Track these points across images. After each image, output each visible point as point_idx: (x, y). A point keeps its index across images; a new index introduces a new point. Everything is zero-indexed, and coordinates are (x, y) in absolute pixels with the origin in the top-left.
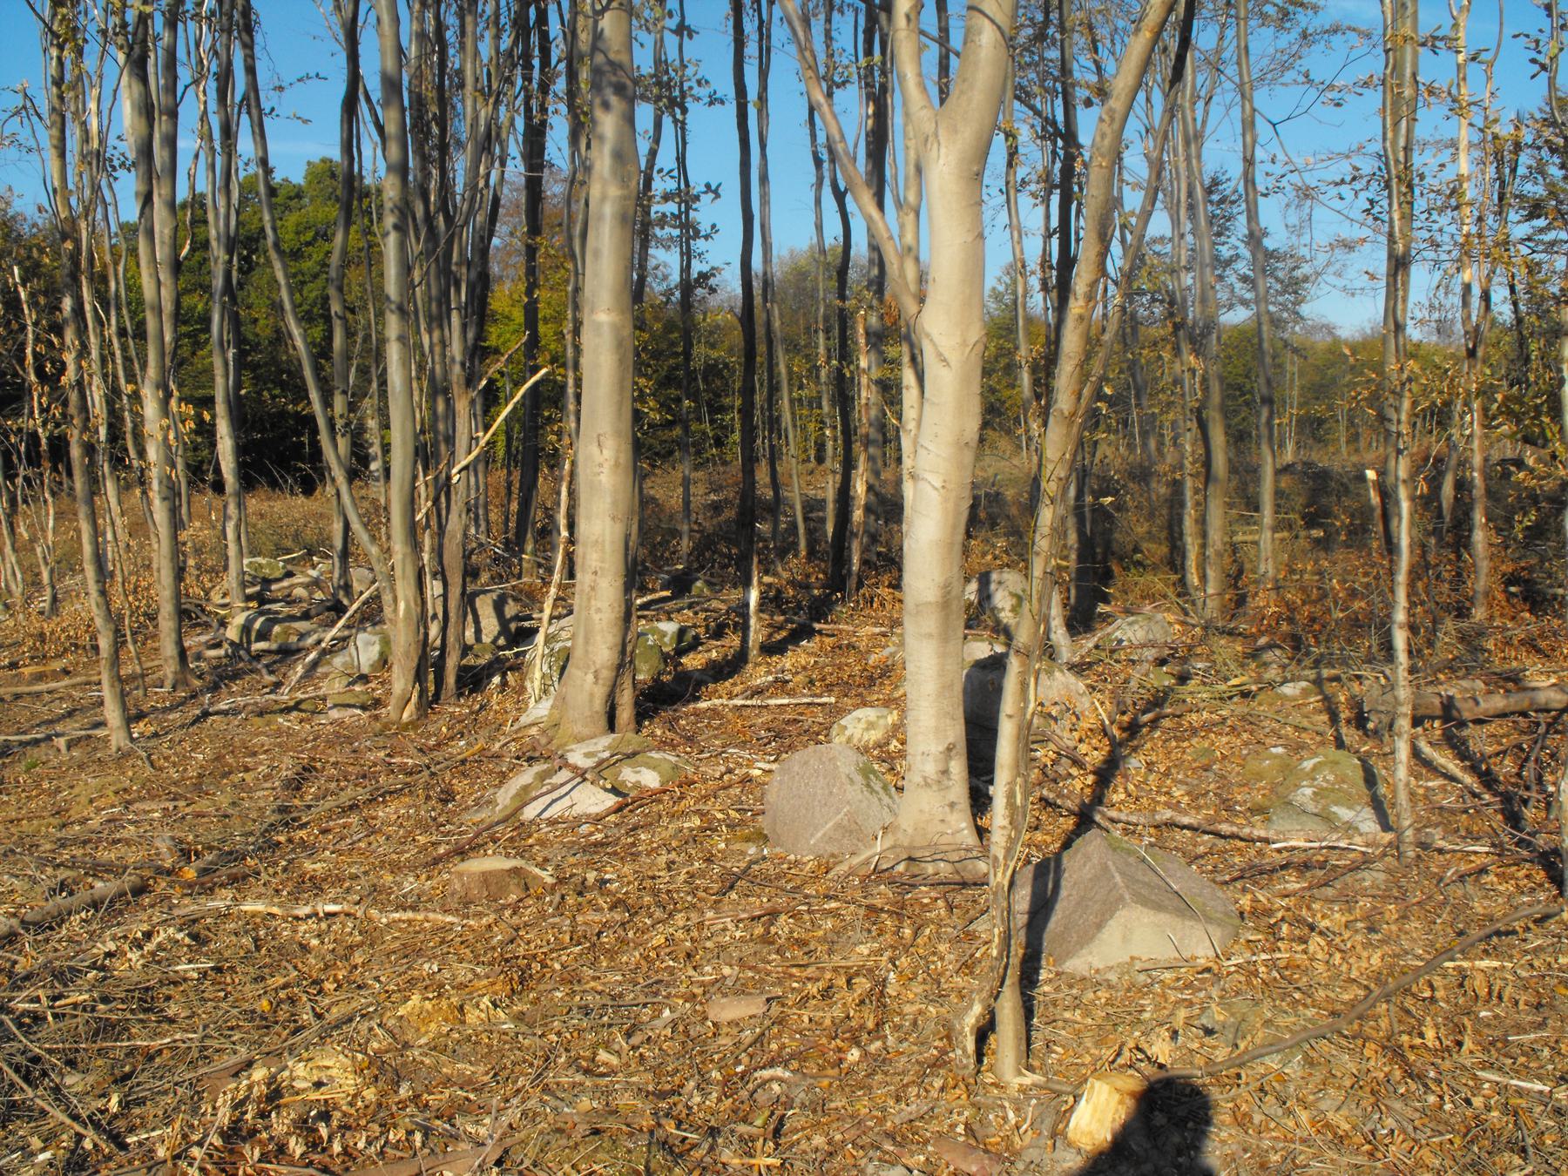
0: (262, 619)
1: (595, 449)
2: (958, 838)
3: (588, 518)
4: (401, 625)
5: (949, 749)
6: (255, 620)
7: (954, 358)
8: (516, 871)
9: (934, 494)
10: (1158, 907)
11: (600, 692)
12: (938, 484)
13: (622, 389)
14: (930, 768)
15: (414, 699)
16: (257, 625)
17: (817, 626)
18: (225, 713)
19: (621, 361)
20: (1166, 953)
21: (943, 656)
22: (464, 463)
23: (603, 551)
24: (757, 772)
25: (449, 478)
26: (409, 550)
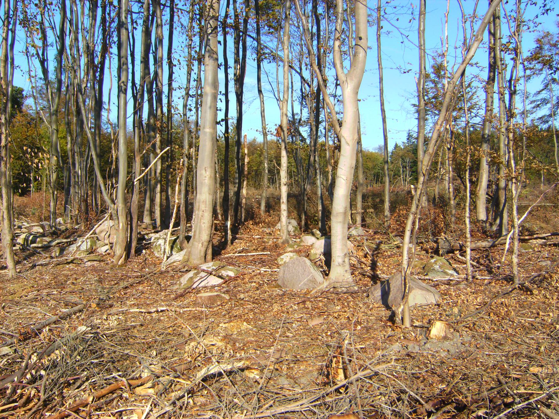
0: (32, 236)
1: (204, 172)
3: (200, 194)
4: (121, 231)
5: (345, 255)
6: (29, 237)
8: (217, 295)
9: (344, 181)
11: (203, 250)
12: (345, 179)
14: (340, 260)
15: (124, 257)
17: (237, 236)
18: (42, 265)
20: (424, 302)
23: (206, 204)
24: (262, 272)
26: (124, 206)
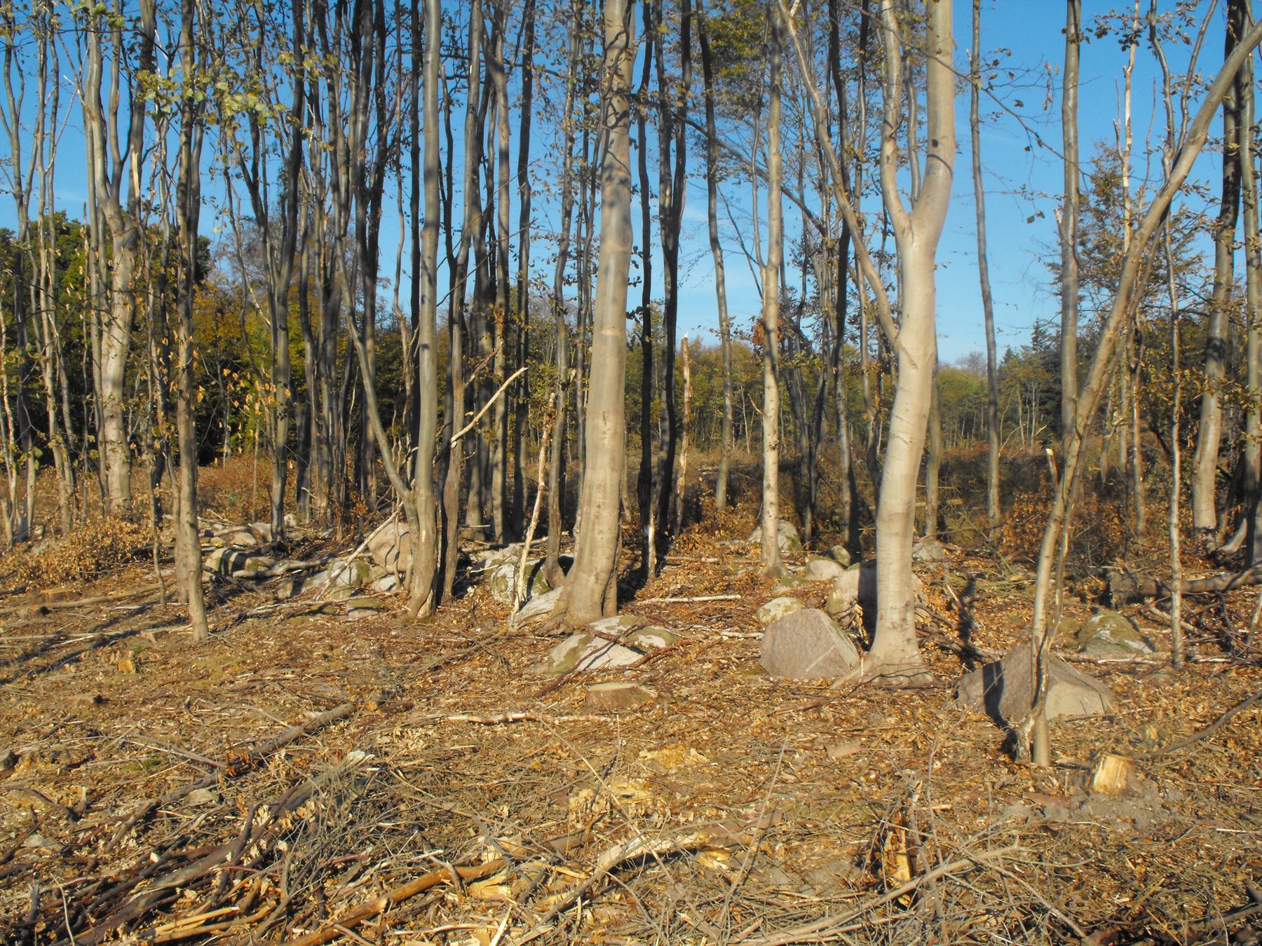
0: (235, 554)
1: (600, 422)
2: (913, 660)
3: (593, 468)
4: (423, 547)
6: (230, 555)
7: (920, 363)
8: (633, 690)
10: (1076, 685)
11: (598, 589)
13: (620, 381)
15: (429, 601)
16: (233, 558)
19: (620, 362)
20: (1079, 712)
21: (903, 546)
22: (461, 433)
23: (605, 491)
25: (449, 444)
